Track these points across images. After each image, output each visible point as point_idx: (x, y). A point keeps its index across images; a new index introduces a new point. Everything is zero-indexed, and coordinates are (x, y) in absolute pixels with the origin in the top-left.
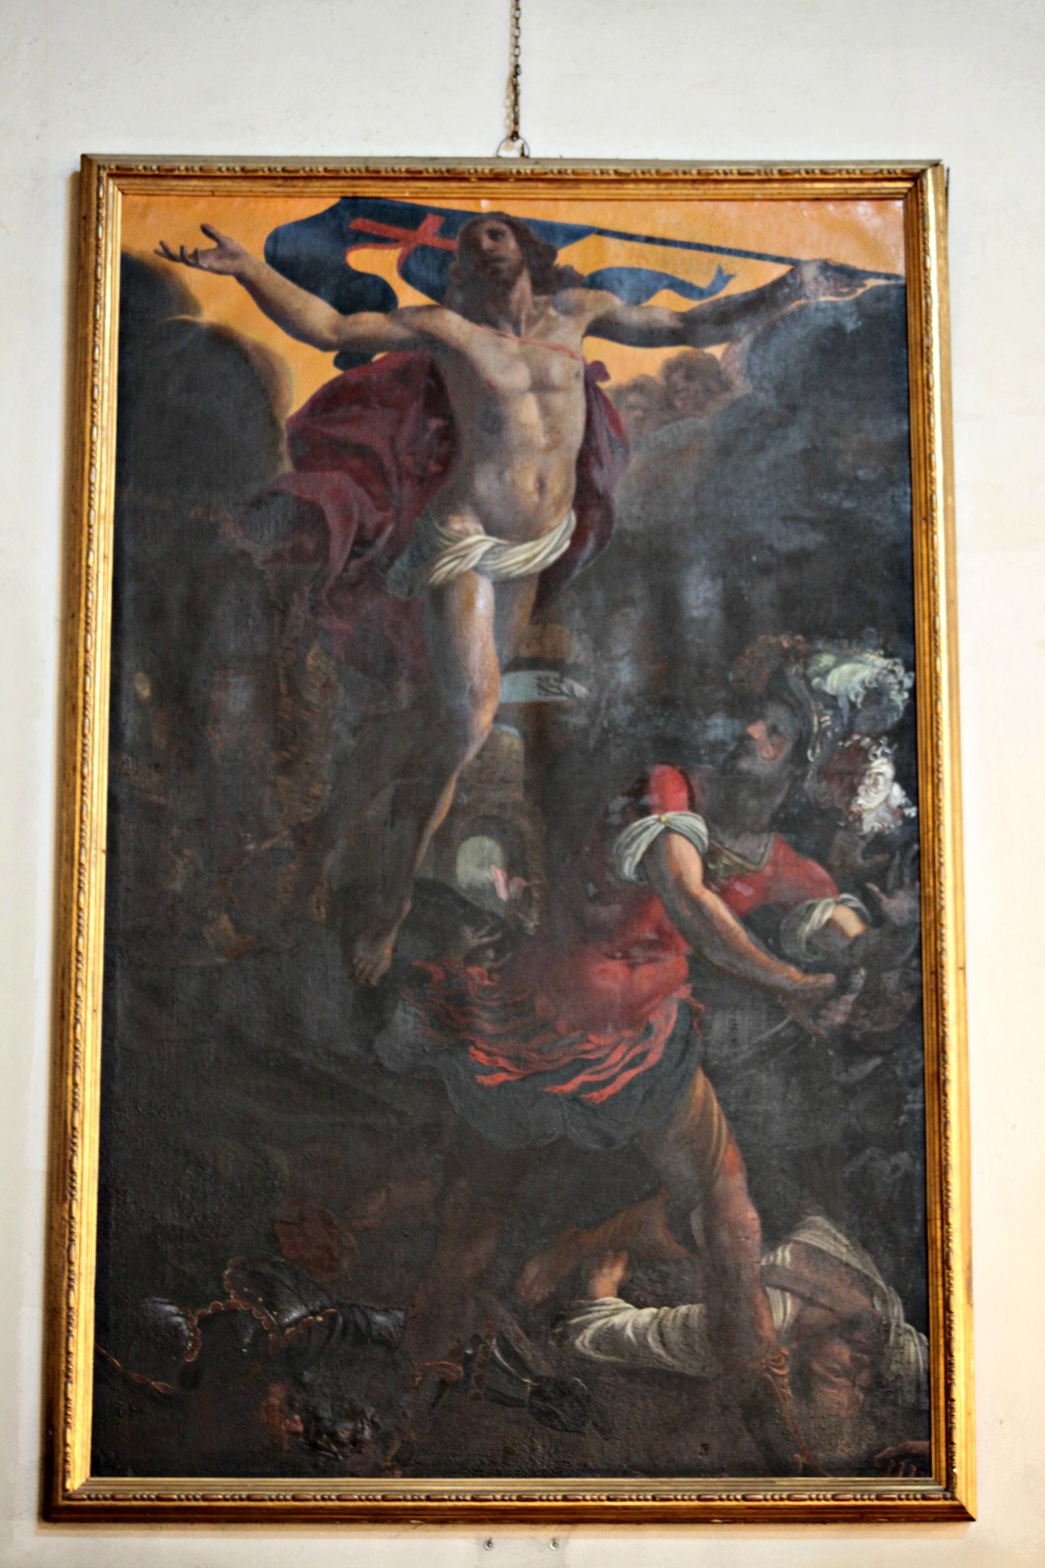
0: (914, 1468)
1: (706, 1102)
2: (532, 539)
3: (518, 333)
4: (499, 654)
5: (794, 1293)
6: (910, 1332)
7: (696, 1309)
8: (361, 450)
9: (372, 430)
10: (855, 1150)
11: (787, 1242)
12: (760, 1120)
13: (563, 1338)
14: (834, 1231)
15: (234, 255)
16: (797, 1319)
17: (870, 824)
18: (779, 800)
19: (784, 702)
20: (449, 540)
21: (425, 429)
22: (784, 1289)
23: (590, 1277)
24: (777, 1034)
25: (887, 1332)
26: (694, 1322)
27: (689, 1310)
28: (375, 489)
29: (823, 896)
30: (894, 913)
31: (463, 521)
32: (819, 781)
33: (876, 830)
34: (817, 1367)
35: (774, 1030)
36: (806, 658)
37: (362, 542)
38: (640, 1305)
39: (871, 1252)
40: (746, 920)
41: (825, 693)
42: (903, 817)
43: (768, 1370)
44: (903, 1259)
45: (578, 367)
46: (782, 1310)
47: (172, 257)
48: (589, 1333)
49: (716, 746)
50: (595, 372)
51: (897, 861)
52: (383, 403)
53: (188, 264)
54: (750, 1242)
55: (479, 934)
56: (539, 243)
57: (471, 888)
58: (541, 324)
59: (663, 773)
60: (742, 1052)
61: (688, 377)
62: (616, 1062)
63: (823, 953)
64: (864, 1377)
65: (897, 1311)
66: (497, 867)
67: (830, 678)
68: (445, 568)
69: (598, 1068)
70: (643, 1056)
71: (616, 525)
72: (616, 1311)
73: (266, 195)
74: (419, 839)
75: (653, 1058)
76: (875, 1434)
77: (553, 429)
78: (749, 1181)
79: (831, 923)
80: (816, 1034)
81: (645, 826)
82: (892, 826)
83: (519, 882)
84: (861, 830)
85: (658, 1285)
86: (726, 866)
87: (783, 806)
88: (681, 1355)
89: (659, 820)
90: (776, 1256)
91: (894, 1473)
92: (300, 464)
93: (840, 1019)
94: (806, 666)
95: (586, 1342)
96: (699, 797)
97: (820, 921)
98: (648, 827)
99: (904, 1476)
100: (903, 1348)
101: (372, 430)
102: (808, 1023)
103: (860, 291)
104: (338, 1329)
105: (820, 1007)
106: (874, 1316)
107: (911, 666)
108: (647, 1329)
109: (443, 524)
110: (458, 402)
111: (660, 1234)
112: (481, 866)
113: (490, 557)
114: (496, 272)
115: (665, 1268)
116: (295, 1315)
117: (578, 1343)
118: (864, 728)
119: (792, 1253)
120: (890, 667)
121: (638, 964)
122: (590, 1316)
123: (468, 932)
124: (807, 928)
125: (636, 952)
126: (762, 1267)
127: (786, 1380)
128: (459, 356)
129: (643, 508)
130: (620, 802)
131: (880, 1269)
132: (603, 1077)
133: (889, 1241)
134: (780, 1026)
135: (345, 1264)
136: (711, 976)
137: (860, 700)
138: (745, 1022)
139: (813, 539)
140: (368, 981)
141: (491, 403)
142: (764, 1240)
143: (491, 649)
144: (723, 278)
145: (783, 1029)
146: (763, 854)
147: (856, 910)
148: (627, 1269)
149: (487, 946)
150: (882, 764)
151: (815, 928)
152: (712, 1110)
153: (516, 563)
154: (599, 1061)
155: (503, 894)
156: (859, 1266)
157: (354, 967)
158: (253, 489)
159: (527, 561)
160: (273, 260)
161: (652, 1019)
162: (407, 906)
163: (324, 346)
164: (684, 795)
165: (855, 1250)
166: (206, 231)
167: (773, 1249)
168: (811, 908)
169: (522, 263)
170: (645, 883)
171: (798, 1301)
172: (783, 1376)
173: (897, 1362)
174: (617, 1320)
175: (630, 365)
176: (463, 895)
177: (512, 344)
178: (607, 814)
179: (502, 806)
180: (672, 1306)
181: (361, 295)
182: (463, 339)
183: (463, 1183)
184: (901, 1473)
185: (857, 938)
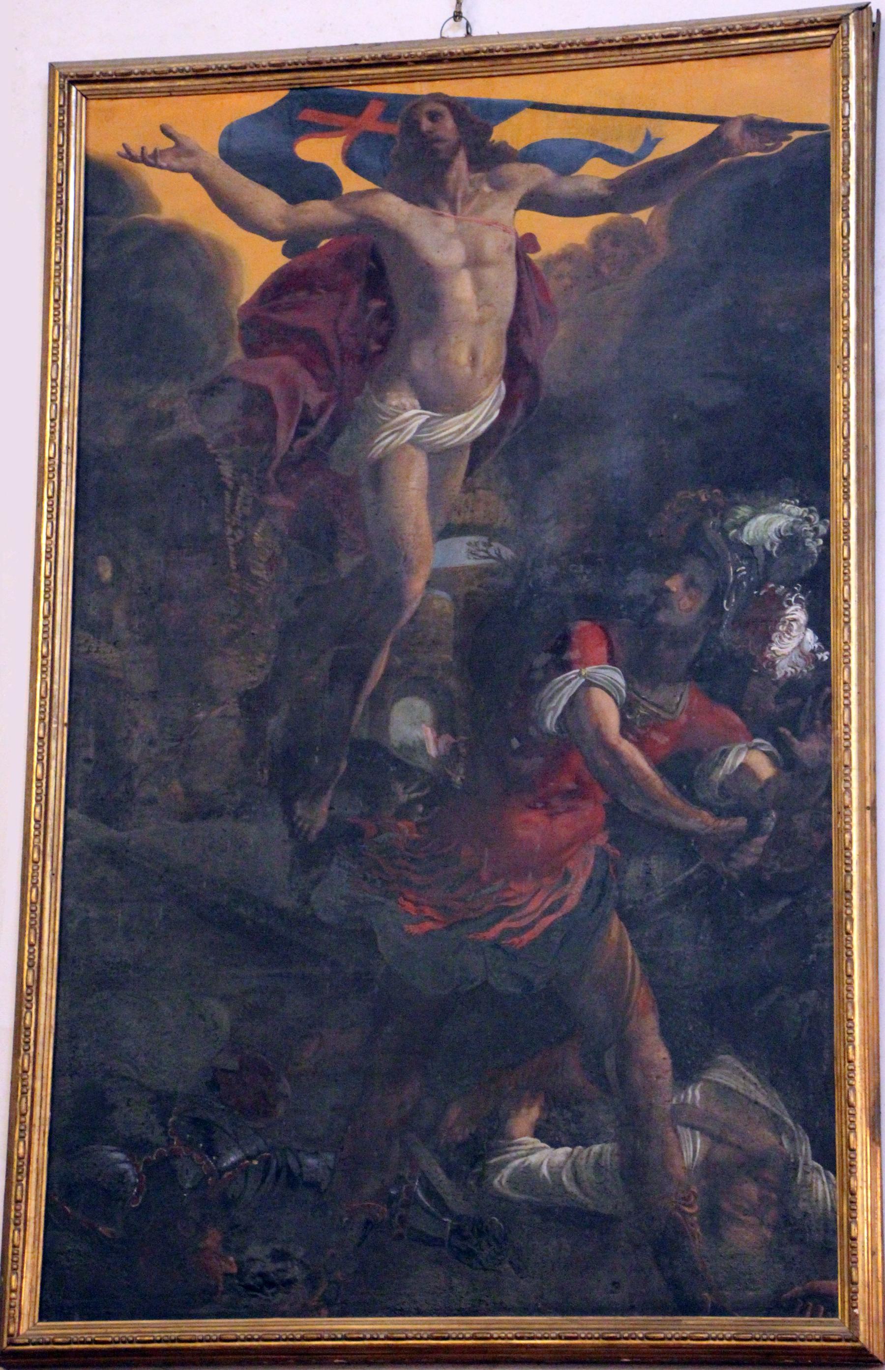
0: (822, 1309)
1: (621, 944)
2: (464, 411)
3: (454, 212)
4: (433, 522)
5: (703, 1131)
6: (818, 1170)
7: (609, 1147)
8: (307, 335)
9: (316, 315)
10: (766, 989)
11: (696, 1082)
12: (673, 963)
13: (481, 1178)
14: (743, 1069)
15: (190, 153)
16: (707, 1158)
17: (783, 669)
18: (695, 649)
19: (702, 555)
20: (388, 416)
21: (366, 310)
22: (693, 1128)
23: (508, 1116)
24: (690, 876)
25: (796, 1170)
26: (607, 1158)
27: (602, 1148)
28: (320, 370)
29: (738, 741)
30: (805, 756)
31: (400, 396)
32: (734, 630)
33: (789, 675)
34: (725, 1205)
35: (687, 873)
36: (723, 512)
37: (306, 421)
38: (555, 1145)
39: (779, 1090)
40: (660, 767)
41: (742, 544)
42: (816, 660)
43: (678, 1209)
44: (811, 1097)
45: (512, 241)
46: (692, 1148)
47: (133, 159)
48: (506, 1172)
49: (632, 603)
50: (528, 243)
51: (808, 705)
52: (329, 289)
53: (149, 164)
54: (660, 1081)
55: (409, 790)
56: (476, 120)
57: (403, 746)
58: (475, 202)
59: (584, 629)
60: (657, 896)
61: (615, 244)
62: (536, 909)
63: (739, 798)
64: (772, 1215)
65: (805, 1148)
66: (427, 726)
67: (746, 529)
68: (385, 441)
69: (518, 915)
70: (561, 902)
71: (544, 391)
72: (532, 1151)
73: (218, 91)
74: (355, 702)
75: (571, 904)
76: (783, 1273)
77: (483, 304)
78: (661, 1022)
79: (744, 767)
80: (730, 877)
81: (567, 679)
82: (805, 671)
83: (447, 738)
84: (774, 675)
85: (573, 1125)
86: (643, 716)
87: (700, 655)
88: (594, 1194)
89: (580, 674)
90: (686, 1094)
91: (802, 1314)
92: (251, 350)
93: (750, 861)
94: (723, 519)
95: (504, 1182)
96: (619, 653)
97: (732, 767)
98: (570, 681)
99: (812, 1316)
100: (811, 1185)
101: (316, 315)
102: (721, 867)
103: (785, 144)
104: (273, 1171)
105: (731, 850)
106: (782, 1153)
107: (825, 514)
108: (562, 1168)
109: (382, 401)
110: (397, 282)
111: (574, 1075)
112: (412, 725)
113: (425, 429)
114: (434, 152)
115: (580, 1108)
116: (233, 1159)
117: (496, 1182)
118: (778, 576)
119: (702, 1092)
120: (805, 515)
121: (559, 813)
122: (508, 1156)
123: (399, 787)
124: (720, 774)
125: (555, 801)
126: (674, 1106)
127: (695, 1218)
128: (399, 239)
129: (569, 374)
130: (542, 659)
131: (788, 1107)
132: (524, 922)
133: (797, 1079)
134: (692, 870)
135: (281, 1110)
136: (631, 826)
137: (775, 549)
138: (657, 865)
139: (731, 394)
140: (305, 838)
141: (428, 283)
142: (676, 1079)
143: (424, 518)
144: (650, 142)
145: (695, 872)
146: (678, 704)
147: (767, 753)
148: (542, 1109)
149: (418, 800)
150: (796, 610)
151: (728, 773)
152: (626, 953)
153: (450, 434)
154: (519, 908)
155: (432, 751)
156: (768, 1105)
157: (293, 825)
158: (207, 376)
159: (461, 431)
160: (228, 155)
161: (570, 865)
162: (343, 766)
163: (273, 236)
164: (604, 649)
165: (764, 1088)
166: (165, 131)
167: (685, 1088)
168: (725, 753)
169: (459, 142)
170: (566, 735)
171: (708, 1139)
172: (691, 1215)
173: (804, 1200)
174: (533, 1159)
175: (559, 234)
176: (395, 753)
177: (448, 223)
178: (531, 670)
179: (433, 668)
180: (586, 1145)
181: (306, 184)
182: (402, 220)
183: (389, 1029)
184: (809, 1313)
185: (768, 781)
